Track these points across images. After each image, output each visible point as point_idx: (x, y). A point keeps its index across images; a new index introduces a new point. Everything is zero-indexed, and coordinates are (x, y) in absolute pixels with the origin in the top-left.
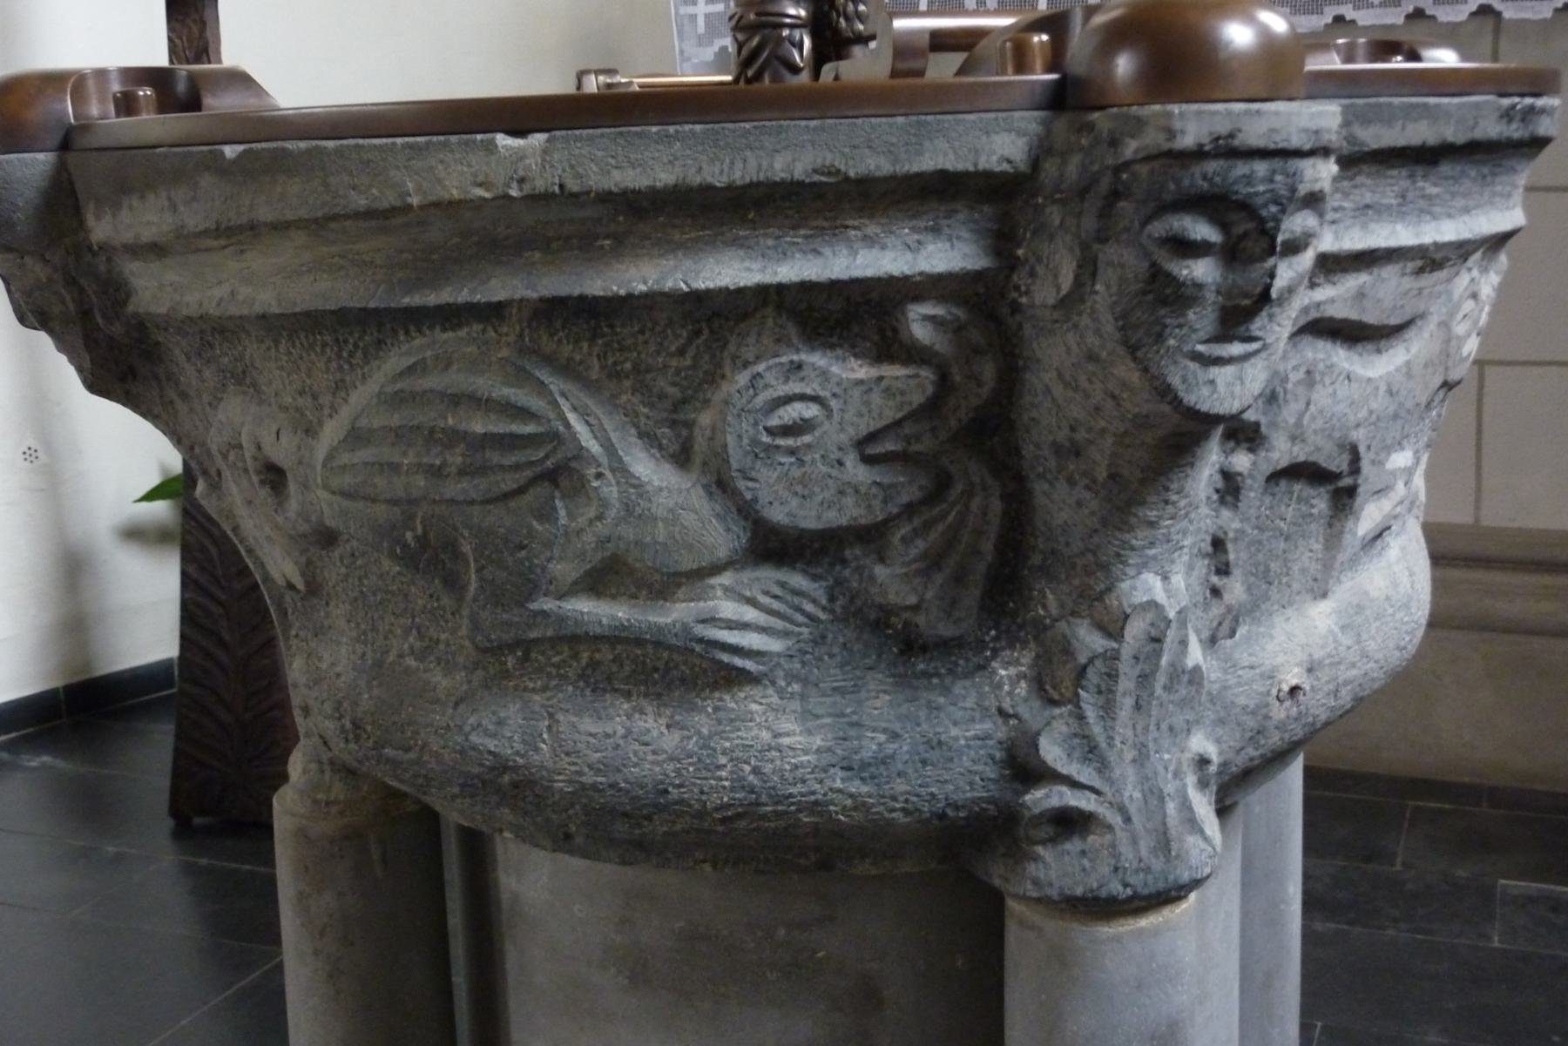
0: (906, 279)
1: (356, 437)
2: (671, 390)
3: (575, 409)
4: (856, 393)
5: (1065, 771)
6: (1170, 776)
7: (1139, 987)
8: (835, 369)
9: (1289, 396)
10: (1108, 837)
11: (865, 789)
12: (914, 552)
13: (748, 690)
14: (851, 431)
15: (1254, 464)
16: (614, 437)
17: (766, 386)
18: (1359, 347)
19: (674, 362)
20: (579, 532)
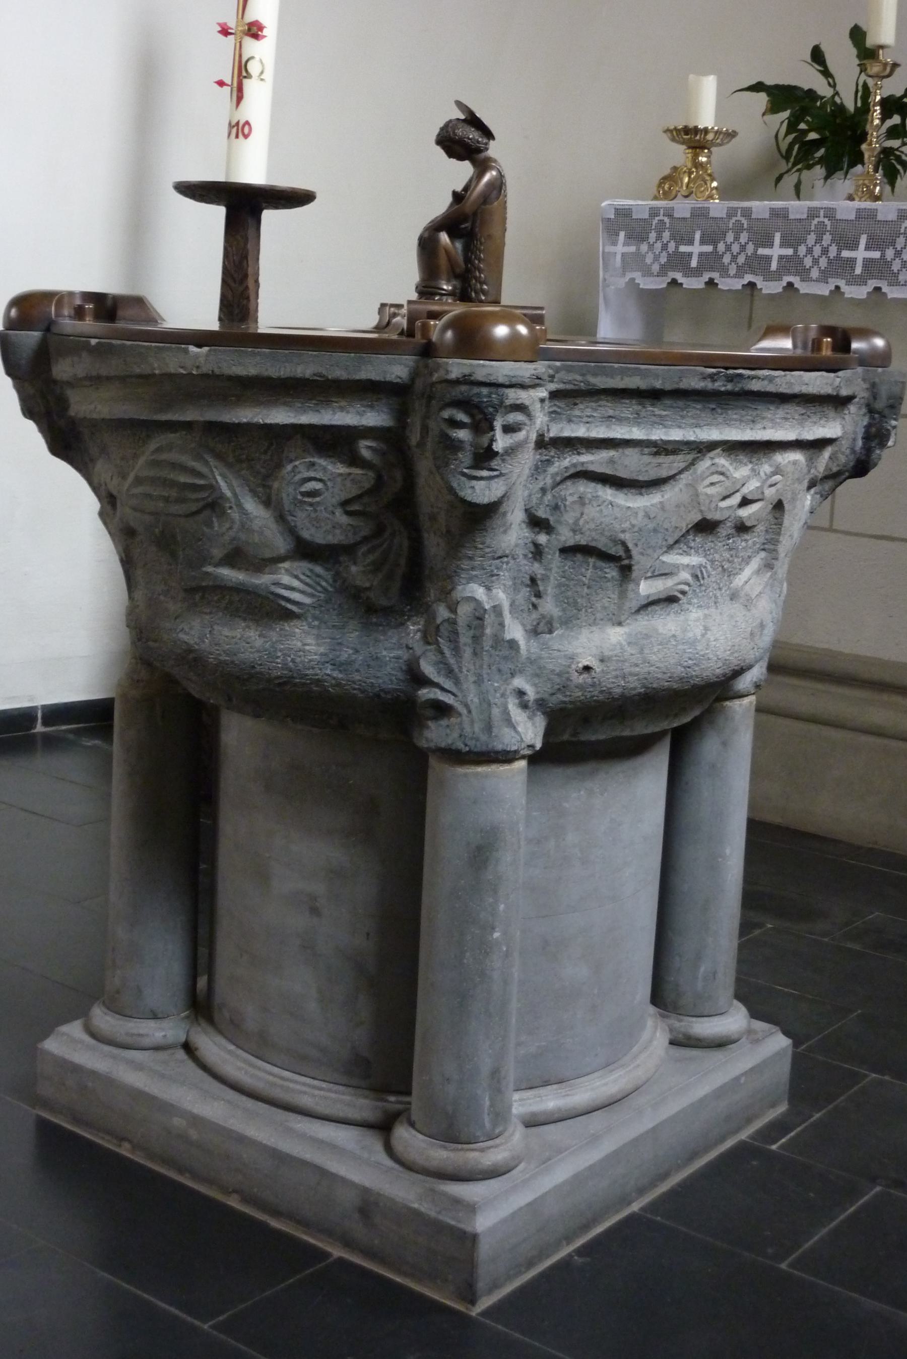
0: (355, 427)
1: (138, 481)
2: (263, 470)
3: (221, 475)
4: (339, 479)
5: (436, 680)
6: (498, 695)
7: (474, 802)
8: (330, 467)
9: (568, 509)
10: (459, 719)
11: (340, 676)
12: (368, 561)
13: (296, 622)
14: (338, 498)
15: (549, 540)
16: (238, 490)
17: (299, 472)
18: (625, 490)
19: (263, 457)
20: (223, 534)
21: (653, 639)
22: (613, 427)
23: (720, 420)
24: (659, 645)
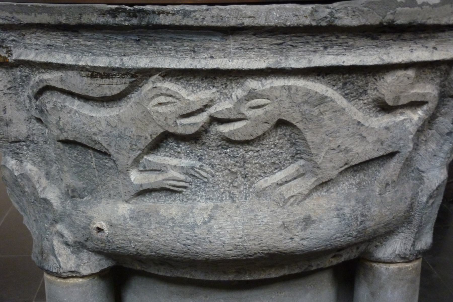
9: (50, 113)
21: (152, 218)
22: (53, 53)
23: (150, 49)
24: (156, 223)
